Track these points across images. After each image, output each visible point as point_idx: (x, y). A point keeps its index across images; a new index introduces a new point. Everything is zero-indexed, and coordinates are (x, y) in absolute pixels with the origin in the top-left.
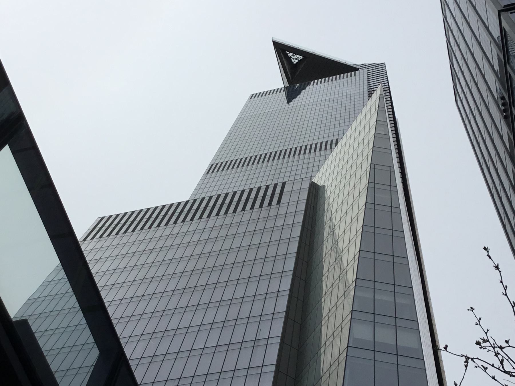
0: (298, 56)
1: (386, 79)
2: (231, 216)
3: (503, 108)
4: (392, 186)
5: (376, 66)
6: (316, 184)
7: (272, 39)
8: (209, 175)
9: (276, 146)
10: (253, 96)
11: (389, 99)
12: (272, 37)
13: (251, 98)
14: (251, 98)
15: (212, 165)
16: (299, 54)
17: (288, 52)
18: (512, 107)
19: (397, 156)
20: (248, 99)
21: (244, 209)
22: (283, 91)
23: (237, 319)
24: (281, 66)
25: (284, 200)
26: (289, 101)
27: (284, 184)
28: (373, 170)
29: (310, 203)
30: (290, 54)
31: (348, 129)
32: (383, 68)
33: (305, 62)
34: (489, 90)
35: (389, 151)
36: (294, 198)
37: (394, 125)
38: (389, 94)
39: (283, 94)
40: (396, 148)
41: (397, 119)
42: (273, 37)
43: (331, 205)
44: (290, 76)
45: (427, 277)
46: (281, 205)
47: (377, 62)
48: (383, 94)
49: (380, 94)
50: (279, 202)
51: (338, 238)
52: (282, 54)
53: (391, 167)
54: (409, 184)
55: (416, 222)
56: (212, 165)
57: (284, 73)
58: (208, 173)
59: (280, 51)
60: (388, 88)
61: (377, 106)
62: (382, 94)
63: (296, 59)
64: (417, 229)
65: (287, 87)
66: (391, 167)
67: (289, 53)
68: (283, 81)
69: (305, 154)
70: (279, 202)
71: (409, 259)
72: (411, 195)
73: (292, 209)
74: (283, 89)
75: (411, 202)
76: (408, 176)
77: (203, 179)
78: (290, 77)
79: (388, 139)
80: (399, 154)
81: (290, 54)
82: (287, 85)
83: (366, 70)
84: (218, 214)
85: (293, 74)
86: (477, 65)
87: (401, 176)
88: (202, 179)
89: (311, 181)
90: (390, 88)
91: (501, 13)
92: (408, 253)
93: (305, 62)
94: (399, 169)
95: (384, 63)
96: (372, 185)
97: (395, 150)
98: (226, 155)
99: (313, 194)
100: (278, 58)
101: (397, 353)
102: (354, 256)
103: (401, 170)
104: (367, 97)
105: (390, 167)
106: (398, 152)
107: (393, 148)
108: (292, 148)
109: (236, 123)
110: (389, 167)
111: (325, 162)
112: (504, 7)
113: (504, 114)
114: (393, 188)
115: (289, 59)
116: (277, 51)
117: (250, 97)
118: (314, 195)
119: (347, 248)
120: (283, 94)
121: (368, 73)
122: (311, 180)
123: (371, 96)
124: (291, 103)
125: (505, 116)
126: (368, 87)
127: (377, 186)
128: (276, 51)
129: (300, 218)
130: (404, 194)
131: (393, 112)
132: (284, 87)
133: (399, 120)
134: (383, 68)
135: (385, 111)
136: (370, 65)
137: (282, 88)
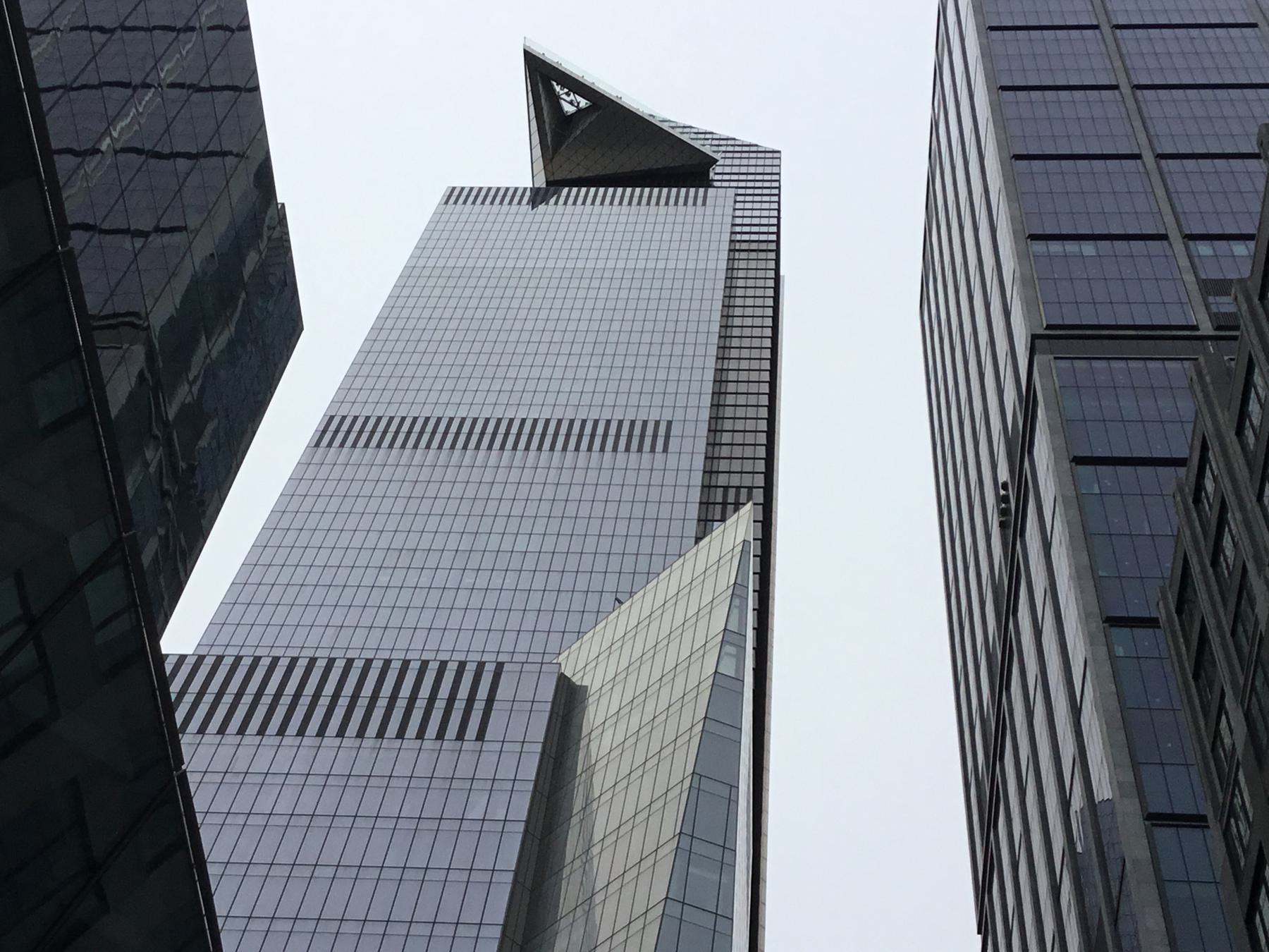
0: (579, 99)
1: (776, 188)
3: (1002, 492)
4: (728, 848)
5: (760, 155)
7: (524, 45)
8: (321, 450)
10: (455, 196)
13: (446, 203)
14: (446, 203)
15: (332, 418)
17: (555, 83)
18: (1004, 693)
20: (439, 204)
22: (528, 204)
27: (500, 666)
28: (694, 792)
29: (547, 751)
33: (594, 117)
34: (1005, 194)
38: (777, 207)
48: (752, 541)
50: (481, 736)
53: (734, 787)
54: (776, 540)
55: (772, 642)
56: (332, 418)
57: (537, 132)
58: (317, 445)
63: (570, 104)
65: (539, 189)
68: (533, 177)
70: (481, 736)
74: (528, 193)
76: (774, 570)
77: (304, 464)
78: (544, 122)
80: (769, 397)
83: (731, 192)
86: (985, 193)
91: (1036, 341)
93: (594, 117)
95: (779, 152)
96: (685, 841)
100: (530, 94)
105: (731, 786)
106: (759, 571)
112: (1046, 329)
113: (1003, 505)
115: (555, 100)
118: (560, 719)
124: (542, 207)
125: (1003, 509)
128: (529, 88)
133: (786, 278)
135: (747, 599)
137: (525, 189)
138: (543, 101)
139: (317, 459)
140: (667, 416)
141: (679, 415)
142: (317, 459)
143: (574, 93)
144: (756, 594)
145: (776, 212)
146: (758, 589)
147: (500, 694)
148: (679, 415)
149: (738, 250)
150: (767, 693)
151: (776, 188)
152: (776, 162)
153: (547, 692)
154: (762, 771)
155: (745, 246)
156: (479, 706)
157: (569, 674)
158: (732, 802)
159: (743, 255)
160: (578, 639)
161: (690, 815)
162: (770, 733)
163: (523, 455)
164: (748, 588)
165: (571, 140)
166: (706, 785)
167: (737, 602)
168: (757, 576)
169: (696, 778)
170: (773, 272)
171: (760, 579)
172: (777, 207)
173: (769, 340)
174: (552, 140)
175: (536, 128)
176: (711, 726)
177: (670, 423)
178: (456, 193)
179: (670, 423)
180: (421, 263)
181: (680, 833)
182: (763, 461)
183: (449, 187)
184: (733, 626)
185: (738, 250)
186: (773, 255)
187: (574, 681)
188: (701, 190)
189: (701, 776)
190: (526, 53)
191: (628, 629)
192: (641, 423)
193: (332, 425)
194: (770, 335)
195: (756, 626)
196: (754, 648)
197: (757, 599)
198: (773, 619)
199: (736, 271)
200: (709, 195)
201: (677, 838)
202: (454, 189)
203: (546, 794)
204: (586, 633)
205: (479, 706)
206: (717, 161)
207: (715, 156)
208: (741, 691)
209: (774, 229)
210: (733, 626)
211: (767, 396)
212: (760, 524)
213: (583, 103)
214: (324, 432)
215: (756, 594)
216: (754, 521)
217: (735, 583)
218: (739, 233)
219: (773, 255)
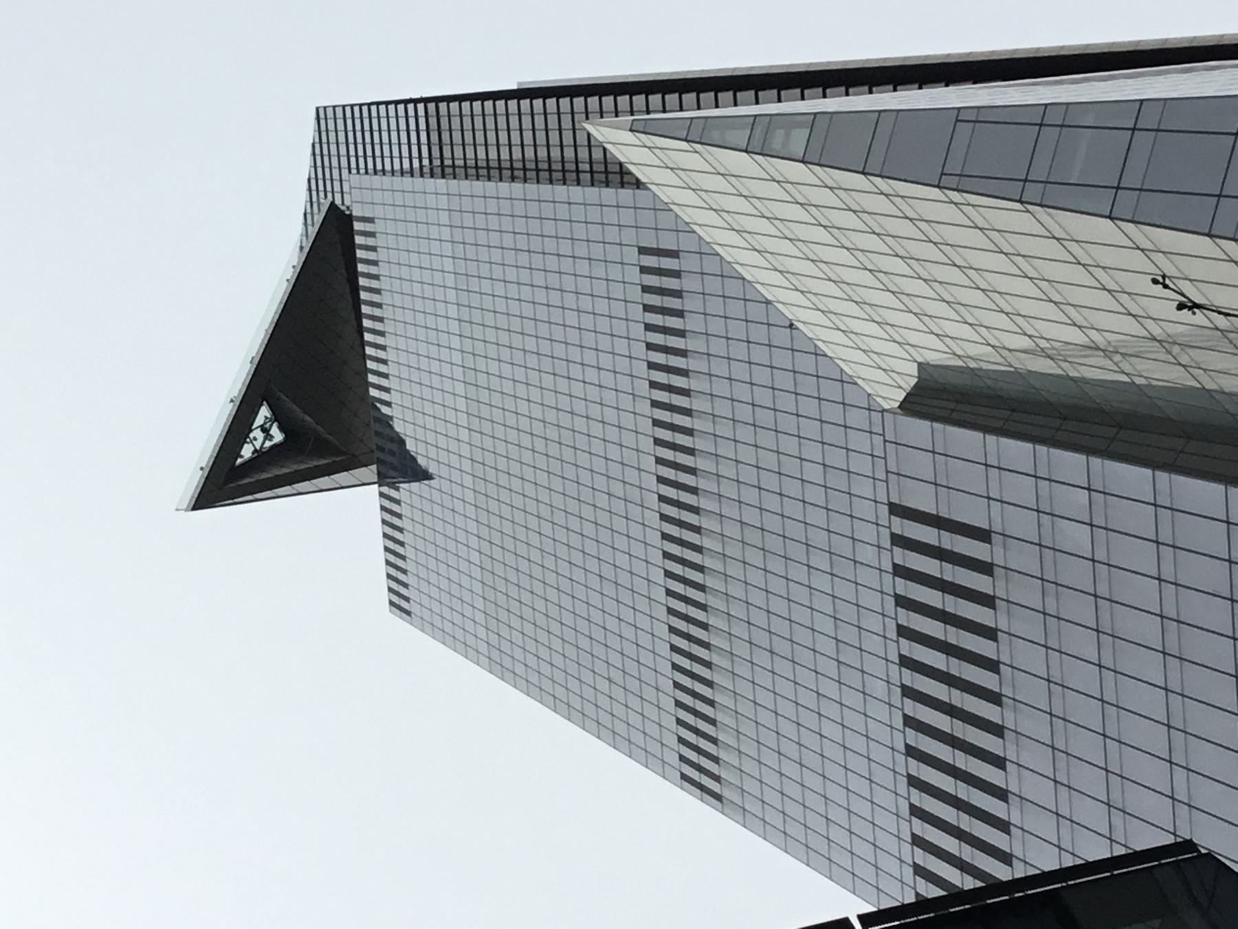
0: (259, 421)
1: (369, 111)
2: (1015, 712)
4: (1042, 118)
5: (324, 139)
6: (908, 394)
7: (186, 510)
8: (726, 793)
9: (512, 549)
10: (400, 604)
11: (466, 105)
12: (177, 510)
13: (408, 613)
14: (408, 613)
15: (684, 777)
16: (251, 421)
17: (239, 461)
19: (867, 91)
20: (411, 624)
21: (992, 666)
22: (397, 489)
23: (1107, 771)
24: (288, 487)
25: (974, 515)
26: (423, 475)
27: (897, 510)
28: (967, 183)
29: (999, 424)
30: (247, 452)
31: (722, 258)
32: (357, 114)
35: (822, 123)
36: (973, 478)
37: (551, 97)
38: (393, 106)
39: (410, 491)
40: (799, 95)
41: (519, 83)
42: (175, 507)
43: (1043, 344)
44: (326, 461)
45: (1111, 40)
46: (997, 527)
47: (308, 132)
49: (631, 130)
50: (983, 535)
51: (990, 348)
52: (245, 481)
53: (959, 116)
55: (1130, 43)
56: (684, 777)
57: (314, 481)
58: (718, 797)
59: (231, 485)
60: (380, 107)
61: (684, 145)
62: (632, 125)
64: (905, 58)
65: (379, 474)
66: (959, 118)
67: (242, 457)
68: (342, 488)
69: (692, 430)
70: (983, 535)
71: (1050, 102)
72: (868, 60)
73: (1022, 489)
74: (385, 490)
75: (897, 64)
77: (743, 815)
79: (978, 111)
80: (741, 90)
81: (247, 452)
82: (370, 472)
83: (355, 178)
84: (999, 762)
85: (320, 447)
87: (917, 86)
88: (744, 820)
89: (899, 411)
90: (408, 97)
92: (1123, 96)
94: (855, 94)
95: (317, 109)
96: (1033, 191)
97: (739, 107)
98: (617, 722)
99: (953, 410)
100: (236, 500)
101: (1113, 188)
102: (1106, 292)
103: (862, 84)
104: (500, 184)
105: (957, 121)
106: (820, 90)
107: (836, 103)
108: (658, 477)
109: (510, 676)
110: (958, 123)
111: (826, 355)
114: (1146, 121)
116: (233, 499)
117: (401, 618)
118: (960, 407)
119: (888, 328)
120: (410, 491)
121: (367, 173)
122: (893, 410)
123: (621, 164)
126: (422, 176)
127: (1038, 173)
128: (250, 498)
129: (1070, 463)
130: (975, 83)
131: (476, 100)
132: (376, 486)
134: (357, 114)
135: (706, 118)
136: (319, 163)
137: (382, 495)
138: (264, 476)
139: (736, 798)
140: (632, 255)
141: (629, 236)
142: (736, 798)
143: (251, 431)
144: (851, 90)
145: (390, 107)
146: (843, 89)
147: (928, 507)
148: (629, 236)
149: (442, 162)
150: (839, 67)
151: (369, 111)
152: (330, 112)
153: (919, 430)
154: (1222, 46)
155: (436, 153)
156: (948, 541)
157: (901, 396)
158: (978, 117)
159: (447, 153)
160: (856, 384)
161: (992, 186)
162: (1140, 42)
163: (703, 477)
164: (692, 119)
165: (320, 429)
166: (954, 166)
167: (716, 136)
168: (806, 92)
169: (946, 181)
170: (451, 104)
171: (764, 89)
172: (393, 106)
173: (651, 97)
174: (324, 458)
175: (307, 483)
176: (874, 165)
177: (643, 251)
178: (395, 599)
179: (643, 251)
180: (483, 648)
181: (1020, 201)
182: (667, 97)
183: (390, 611)
184: (741, 138)
185: (442, 162)
186: (443, 106)
187: (910, 389)
188: (357, 226)
189: (942, 174)
190: (195, 508)
191: (967, 282)
192: (646, 295)
193: (692, 776)
194: (643, 96)
195: (891, 87)
196: (920, 88)
197: (880, 88)
198: (1044, 49)
199: (468, 162)
200: (360, 214)
201: (1030, 207)
202: (392, 603)
203: (1058, 422)
204: (842, 370)
205: (948, 541)
206: (333, 203)
207: (324, 209)
208: (895, 113)
209: (382, 108)
210: (741, 138)
211: (720, 95)
212: (760, 93)
213: (264, 412)
214: (702, 788)
215: (851, 90)
216: (757, 103)
217: (686, 140)
218: (421, 161)
219: (443, 106)
